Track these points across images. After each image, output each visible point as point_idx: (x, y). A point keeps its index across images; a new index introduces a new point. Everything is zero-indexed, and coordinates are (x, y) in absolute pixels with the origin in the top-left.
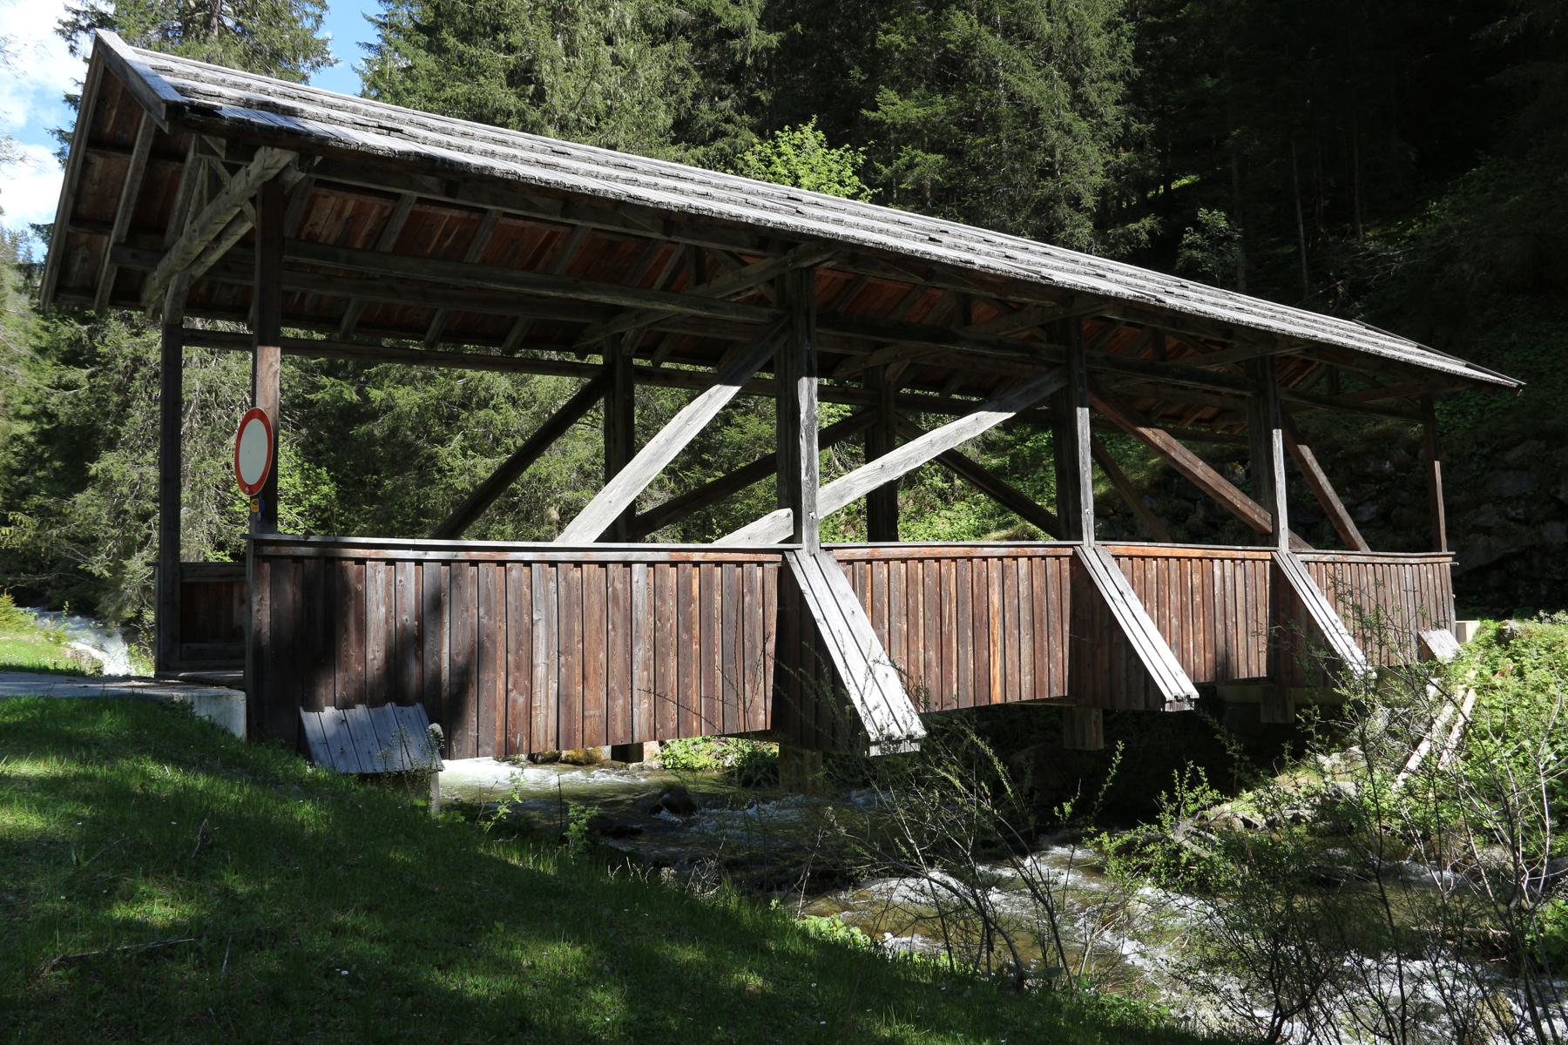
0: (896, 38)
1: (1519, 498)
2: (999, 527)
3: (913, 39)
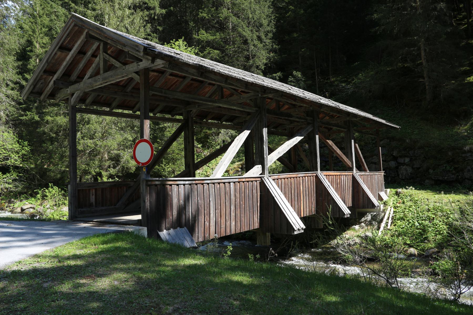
0: (205, 15)
2: (238, 161)
3: (210, 16)
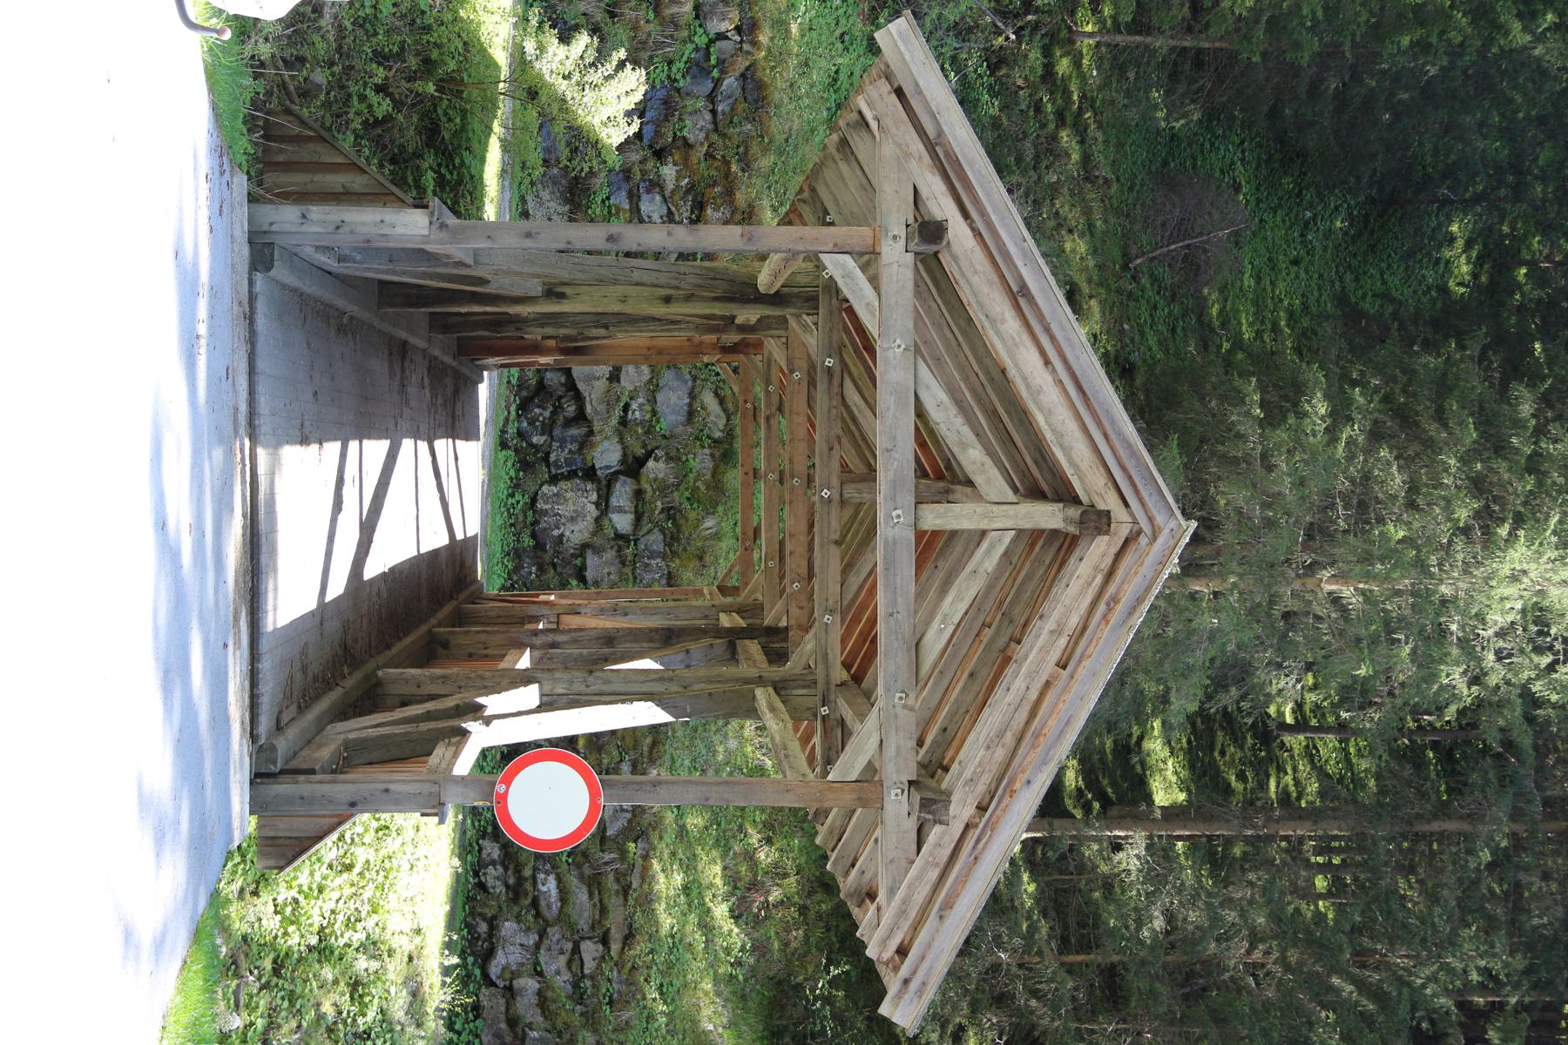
1: (654, 413)
